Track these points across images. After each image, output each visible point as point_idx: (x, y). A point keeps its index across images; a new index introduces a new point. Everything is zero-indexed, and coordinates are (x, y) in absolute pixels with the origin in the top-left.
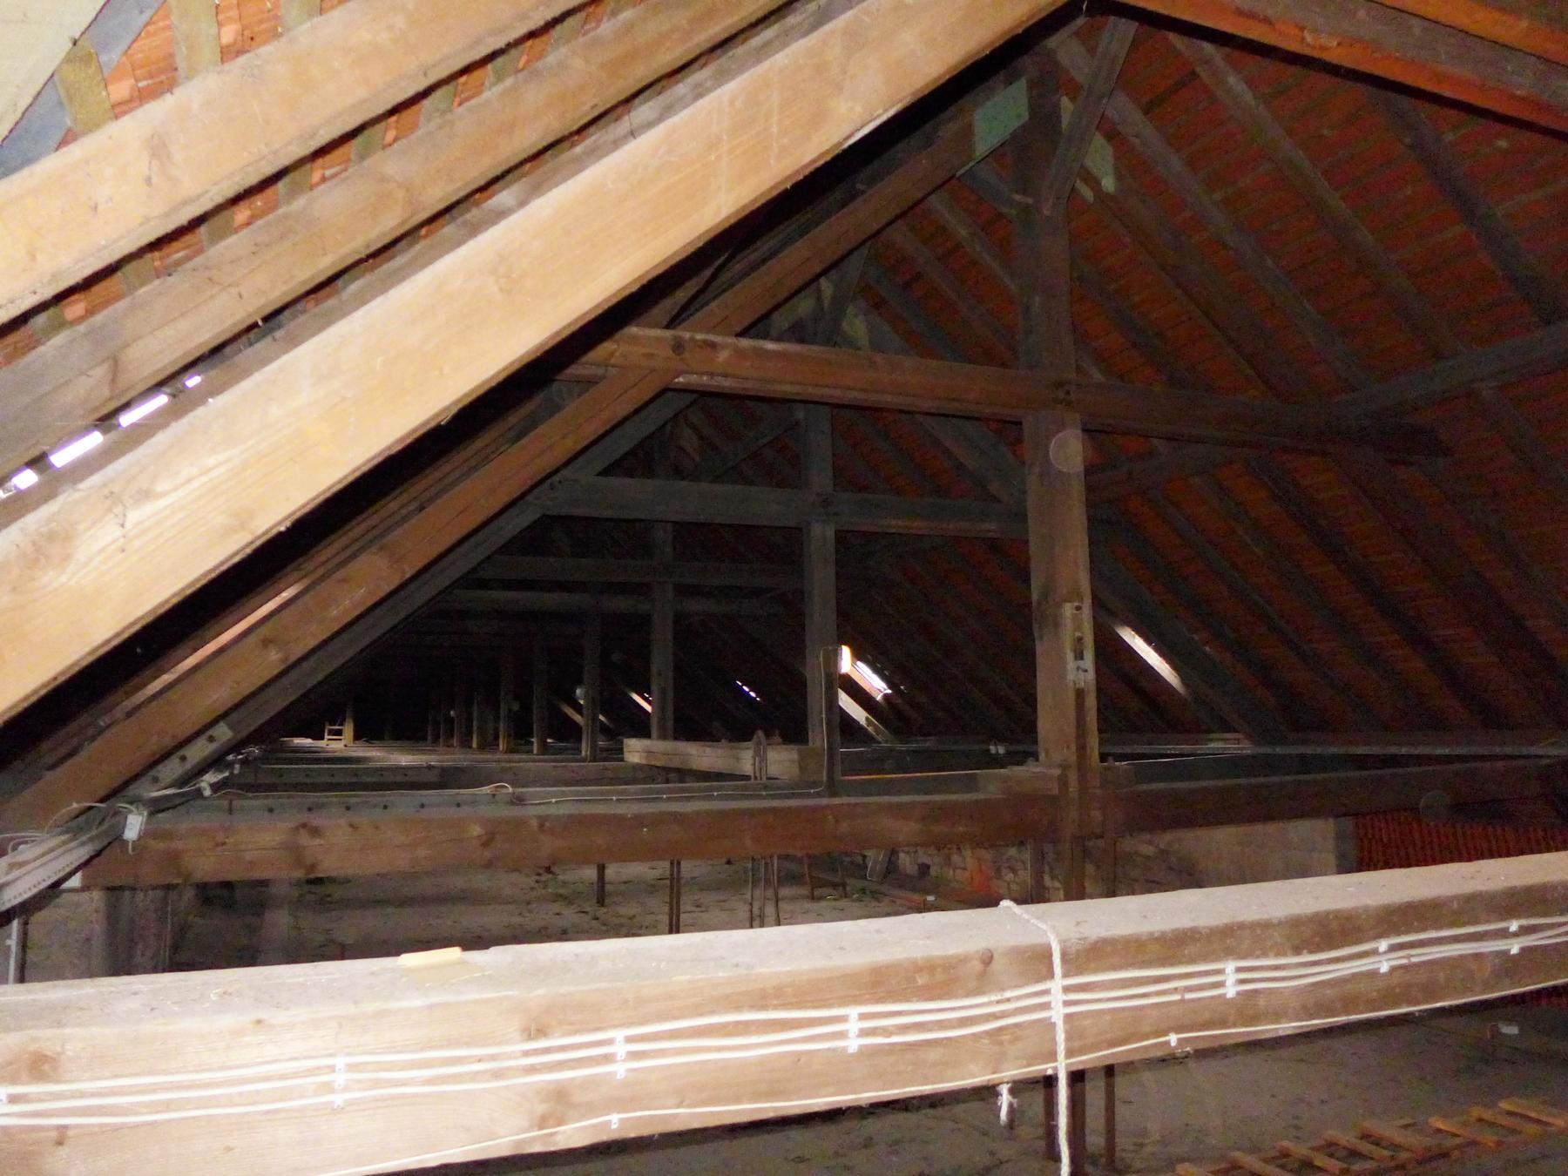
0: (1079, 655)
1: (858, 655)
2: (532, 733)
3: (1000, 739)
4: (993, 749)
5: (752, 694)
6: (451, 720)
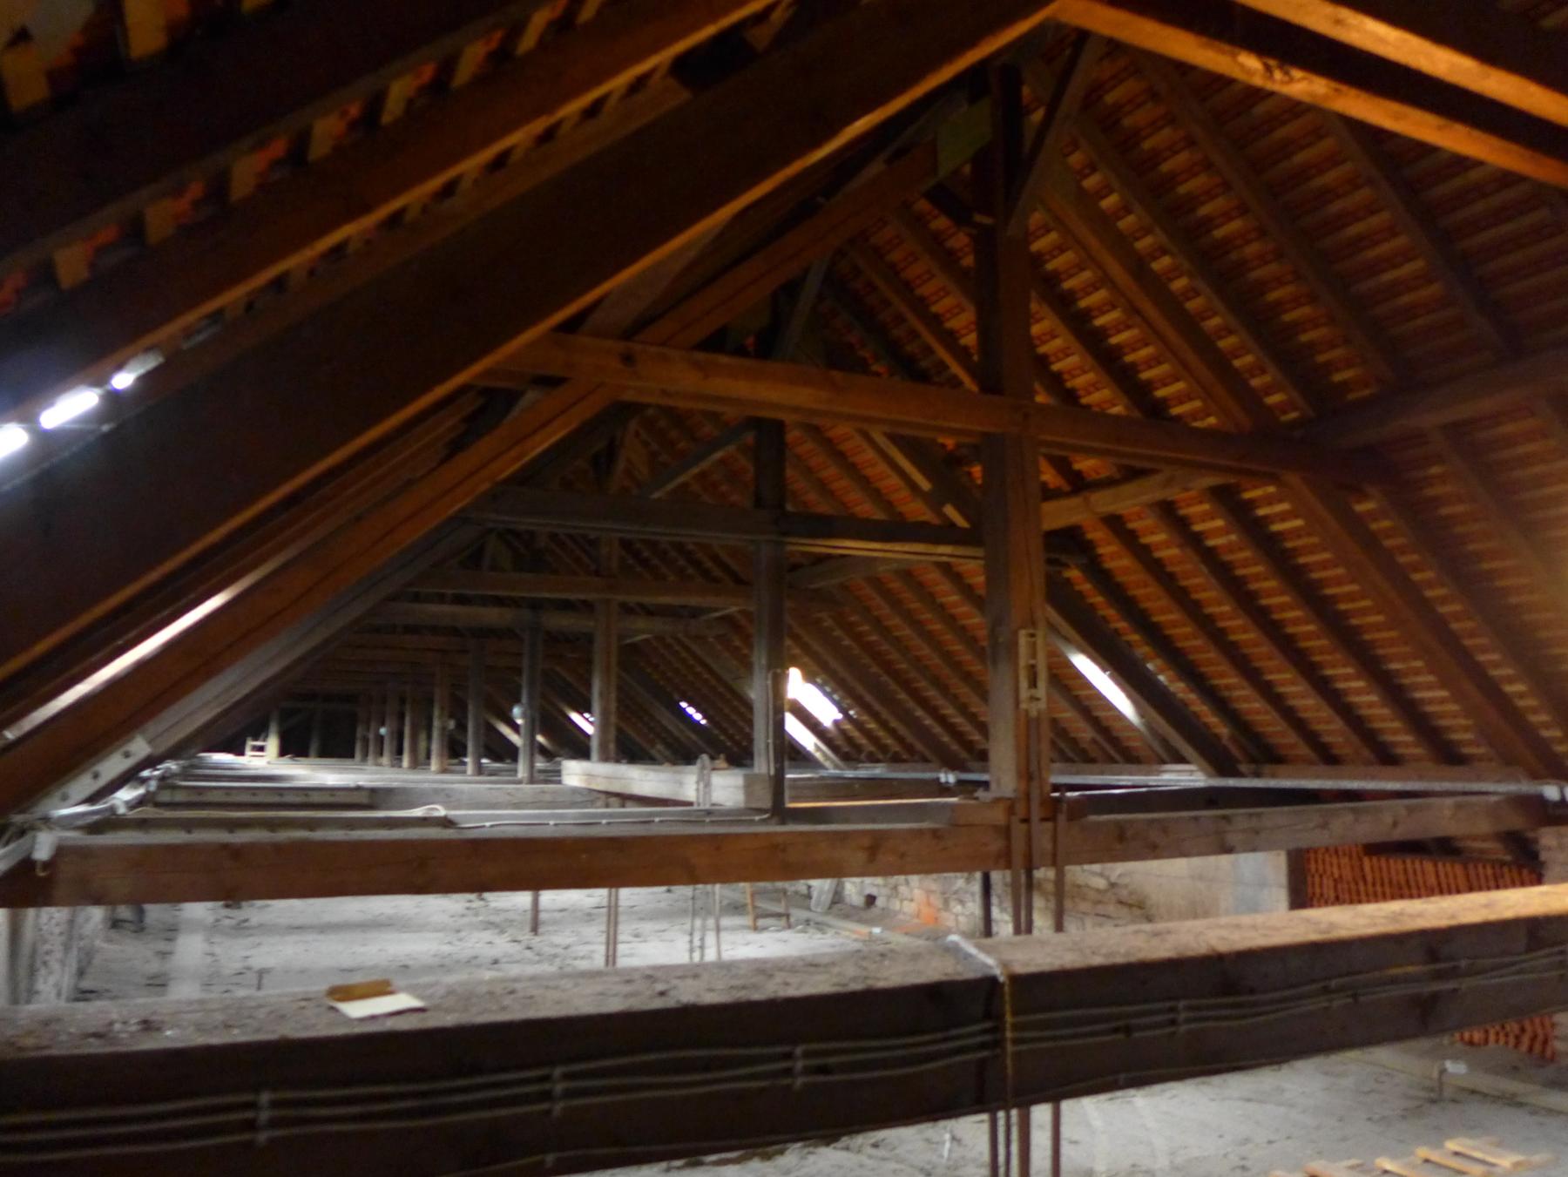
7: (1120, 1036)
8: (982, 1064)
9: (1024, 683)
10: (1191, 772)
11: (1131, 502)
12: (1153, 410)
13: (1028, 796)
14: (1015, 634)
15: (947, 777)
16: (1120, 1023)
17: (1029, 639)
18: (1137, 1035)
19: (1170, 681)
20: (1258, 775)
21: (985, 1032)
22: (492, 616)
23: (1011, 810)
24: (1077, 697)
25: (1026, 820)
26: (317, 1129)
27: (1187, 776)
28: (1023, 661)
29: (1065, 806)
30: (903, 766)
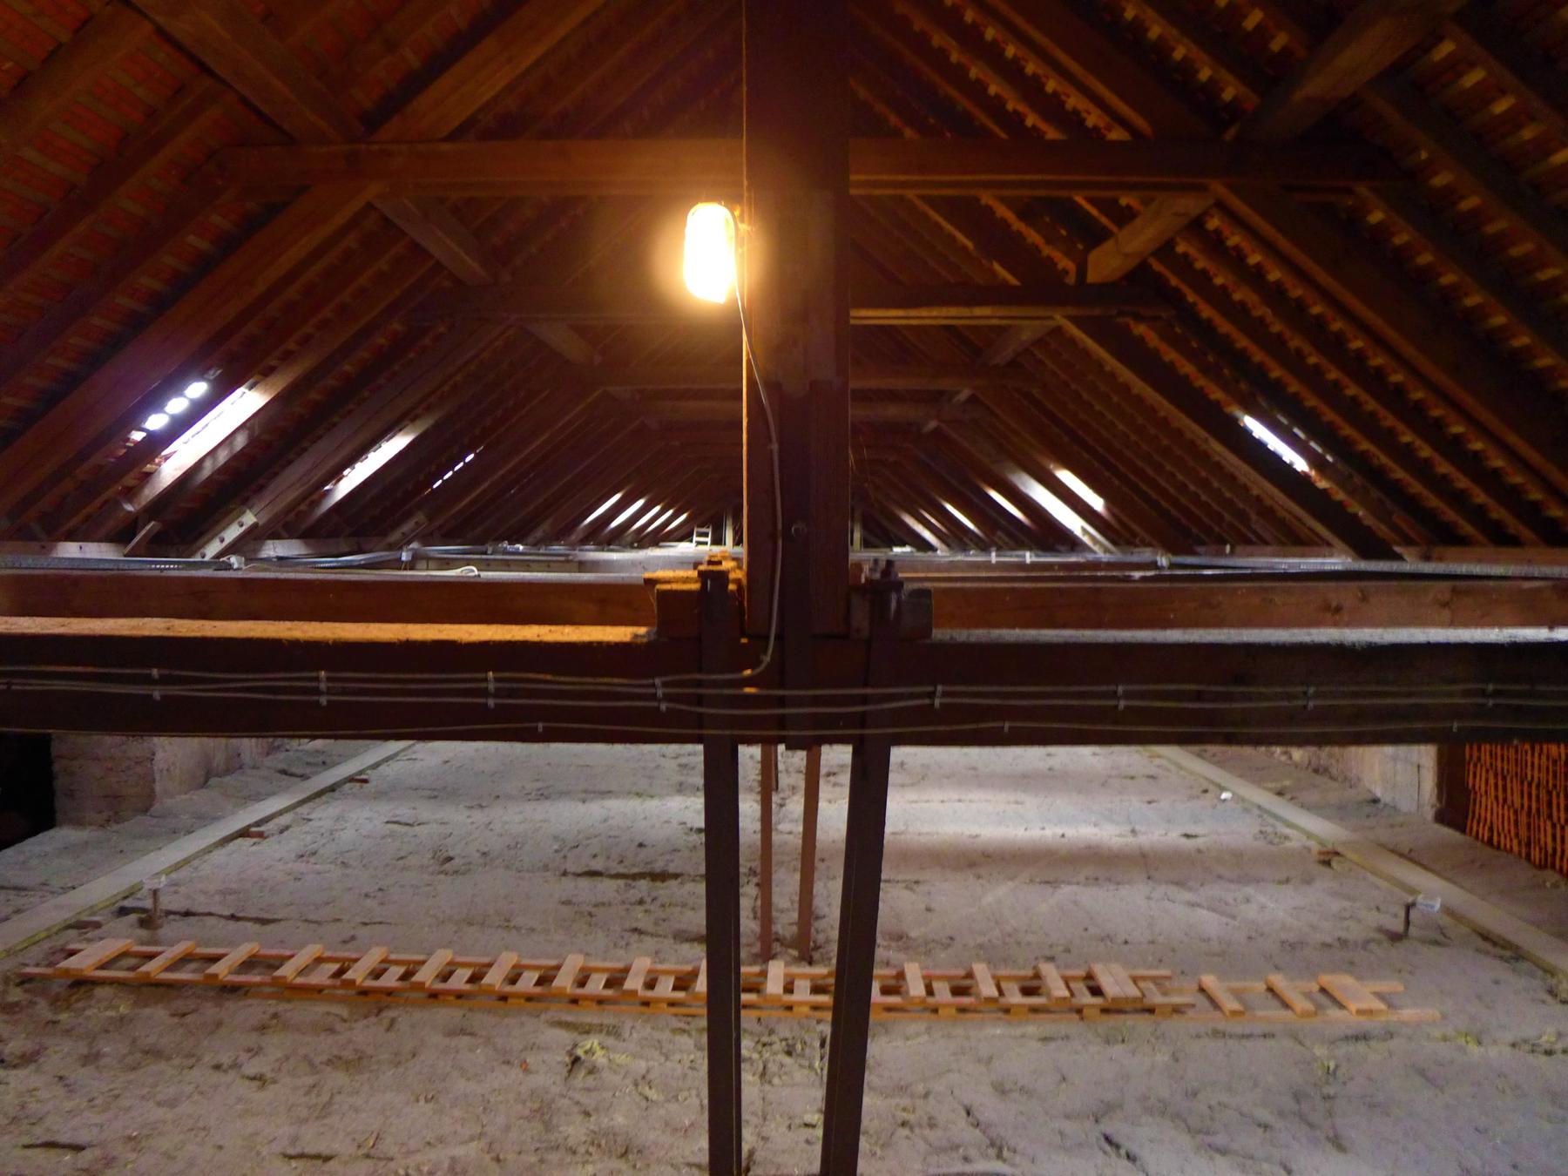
3: (1171, 549)
4: (1158, 559)
15: (1161, 560)
27: (1338, 561)
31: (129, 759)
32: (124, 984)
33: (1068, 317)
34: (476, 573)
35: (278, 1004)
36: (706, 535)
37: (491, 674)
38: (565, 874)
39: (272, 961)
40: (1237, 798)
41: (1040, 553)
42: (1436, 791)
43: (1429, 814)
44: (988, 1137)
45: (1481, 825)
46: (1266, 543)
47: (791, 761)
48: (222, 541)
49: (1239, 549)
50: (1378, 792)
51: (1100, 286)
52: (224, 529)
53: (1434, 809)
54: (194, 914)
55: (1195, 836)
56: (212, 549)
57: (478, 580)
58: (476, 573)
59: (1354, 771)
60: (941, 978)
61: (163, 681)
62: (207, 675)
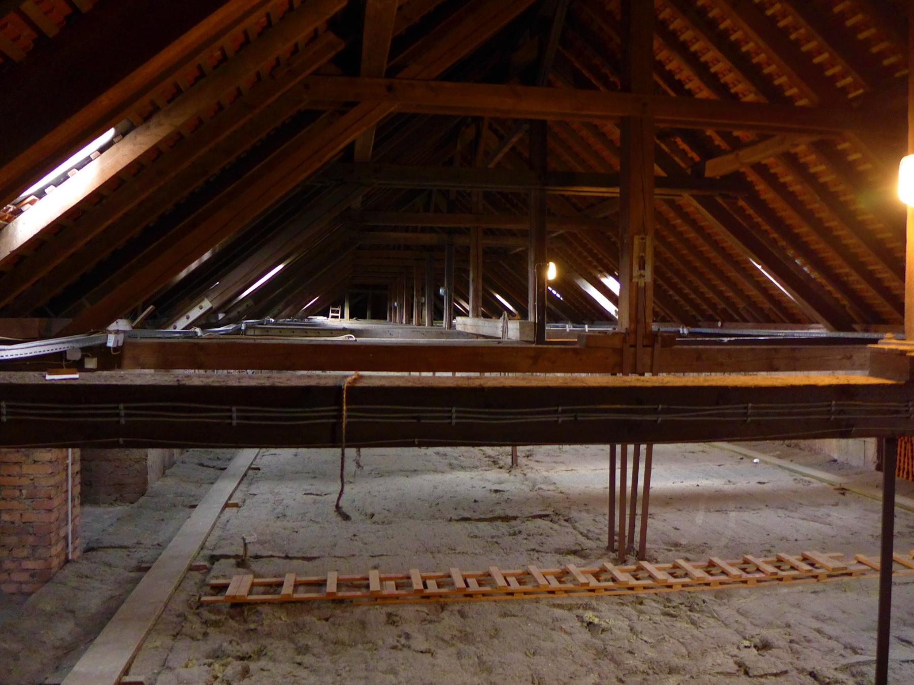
0: (642, 267)
1: (50, 374)
2: (347, 390)
3: (686, 324)
4: (681, 330)
5: (558, 296)
6: (395, 308)
7: (415, 421)
8: (334, 425)
9: (636, 267)
10: (819, 328)
11: (766, 154)
12: (773, 93)
13: (635, 332)
14: (632, 238)
15: (683, 331)
16: (416, 415)
17: (641, 241)
18: (422, 421)
19: (811, 271)
20: (867, 330)
21: (334, 411)
22: (427, 239)
23: (624, 340)
24: (758, 282)
25: (634, 346)
26: (24, 417)
27: (819, 331)
28: (635, 255)
29: (660, 339)
30: (667, 324)
31: (130, 459)
32: (273, 603)
33: (693, 196)
34: (354, 339)
35: (334, 608)
36: (338, 312)
37: (750, 405)
38: (450, 520)
39: (321, 582)
40: (761, 461)
41: (576, 325)
42: (876, 454)
43: (873, 467)
44: (841, 644)
45: (901, 471)
46: (784, 322)
47: (631, 448)
48: (188, 318)
49: (727, 324)
50: (836, 456)
51: (712, 180)
52: (190, 310)
53: (875, 465)
54: (261, 557)
55: (764, 483)
56: (181, 324)
57: (356, 343)
58: (354, 339)
59: (818, 445)
60: (431, 578)
61: (664, 412)
62: (690, 408)
